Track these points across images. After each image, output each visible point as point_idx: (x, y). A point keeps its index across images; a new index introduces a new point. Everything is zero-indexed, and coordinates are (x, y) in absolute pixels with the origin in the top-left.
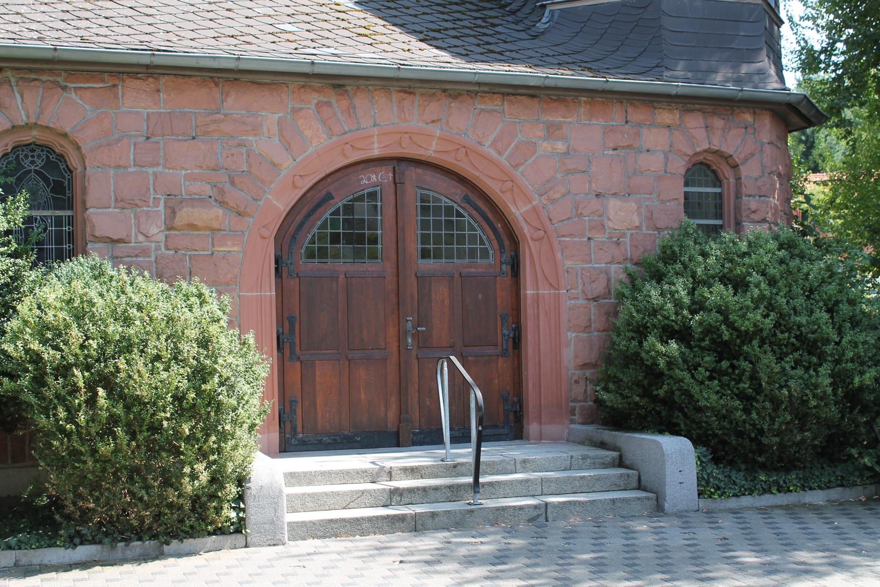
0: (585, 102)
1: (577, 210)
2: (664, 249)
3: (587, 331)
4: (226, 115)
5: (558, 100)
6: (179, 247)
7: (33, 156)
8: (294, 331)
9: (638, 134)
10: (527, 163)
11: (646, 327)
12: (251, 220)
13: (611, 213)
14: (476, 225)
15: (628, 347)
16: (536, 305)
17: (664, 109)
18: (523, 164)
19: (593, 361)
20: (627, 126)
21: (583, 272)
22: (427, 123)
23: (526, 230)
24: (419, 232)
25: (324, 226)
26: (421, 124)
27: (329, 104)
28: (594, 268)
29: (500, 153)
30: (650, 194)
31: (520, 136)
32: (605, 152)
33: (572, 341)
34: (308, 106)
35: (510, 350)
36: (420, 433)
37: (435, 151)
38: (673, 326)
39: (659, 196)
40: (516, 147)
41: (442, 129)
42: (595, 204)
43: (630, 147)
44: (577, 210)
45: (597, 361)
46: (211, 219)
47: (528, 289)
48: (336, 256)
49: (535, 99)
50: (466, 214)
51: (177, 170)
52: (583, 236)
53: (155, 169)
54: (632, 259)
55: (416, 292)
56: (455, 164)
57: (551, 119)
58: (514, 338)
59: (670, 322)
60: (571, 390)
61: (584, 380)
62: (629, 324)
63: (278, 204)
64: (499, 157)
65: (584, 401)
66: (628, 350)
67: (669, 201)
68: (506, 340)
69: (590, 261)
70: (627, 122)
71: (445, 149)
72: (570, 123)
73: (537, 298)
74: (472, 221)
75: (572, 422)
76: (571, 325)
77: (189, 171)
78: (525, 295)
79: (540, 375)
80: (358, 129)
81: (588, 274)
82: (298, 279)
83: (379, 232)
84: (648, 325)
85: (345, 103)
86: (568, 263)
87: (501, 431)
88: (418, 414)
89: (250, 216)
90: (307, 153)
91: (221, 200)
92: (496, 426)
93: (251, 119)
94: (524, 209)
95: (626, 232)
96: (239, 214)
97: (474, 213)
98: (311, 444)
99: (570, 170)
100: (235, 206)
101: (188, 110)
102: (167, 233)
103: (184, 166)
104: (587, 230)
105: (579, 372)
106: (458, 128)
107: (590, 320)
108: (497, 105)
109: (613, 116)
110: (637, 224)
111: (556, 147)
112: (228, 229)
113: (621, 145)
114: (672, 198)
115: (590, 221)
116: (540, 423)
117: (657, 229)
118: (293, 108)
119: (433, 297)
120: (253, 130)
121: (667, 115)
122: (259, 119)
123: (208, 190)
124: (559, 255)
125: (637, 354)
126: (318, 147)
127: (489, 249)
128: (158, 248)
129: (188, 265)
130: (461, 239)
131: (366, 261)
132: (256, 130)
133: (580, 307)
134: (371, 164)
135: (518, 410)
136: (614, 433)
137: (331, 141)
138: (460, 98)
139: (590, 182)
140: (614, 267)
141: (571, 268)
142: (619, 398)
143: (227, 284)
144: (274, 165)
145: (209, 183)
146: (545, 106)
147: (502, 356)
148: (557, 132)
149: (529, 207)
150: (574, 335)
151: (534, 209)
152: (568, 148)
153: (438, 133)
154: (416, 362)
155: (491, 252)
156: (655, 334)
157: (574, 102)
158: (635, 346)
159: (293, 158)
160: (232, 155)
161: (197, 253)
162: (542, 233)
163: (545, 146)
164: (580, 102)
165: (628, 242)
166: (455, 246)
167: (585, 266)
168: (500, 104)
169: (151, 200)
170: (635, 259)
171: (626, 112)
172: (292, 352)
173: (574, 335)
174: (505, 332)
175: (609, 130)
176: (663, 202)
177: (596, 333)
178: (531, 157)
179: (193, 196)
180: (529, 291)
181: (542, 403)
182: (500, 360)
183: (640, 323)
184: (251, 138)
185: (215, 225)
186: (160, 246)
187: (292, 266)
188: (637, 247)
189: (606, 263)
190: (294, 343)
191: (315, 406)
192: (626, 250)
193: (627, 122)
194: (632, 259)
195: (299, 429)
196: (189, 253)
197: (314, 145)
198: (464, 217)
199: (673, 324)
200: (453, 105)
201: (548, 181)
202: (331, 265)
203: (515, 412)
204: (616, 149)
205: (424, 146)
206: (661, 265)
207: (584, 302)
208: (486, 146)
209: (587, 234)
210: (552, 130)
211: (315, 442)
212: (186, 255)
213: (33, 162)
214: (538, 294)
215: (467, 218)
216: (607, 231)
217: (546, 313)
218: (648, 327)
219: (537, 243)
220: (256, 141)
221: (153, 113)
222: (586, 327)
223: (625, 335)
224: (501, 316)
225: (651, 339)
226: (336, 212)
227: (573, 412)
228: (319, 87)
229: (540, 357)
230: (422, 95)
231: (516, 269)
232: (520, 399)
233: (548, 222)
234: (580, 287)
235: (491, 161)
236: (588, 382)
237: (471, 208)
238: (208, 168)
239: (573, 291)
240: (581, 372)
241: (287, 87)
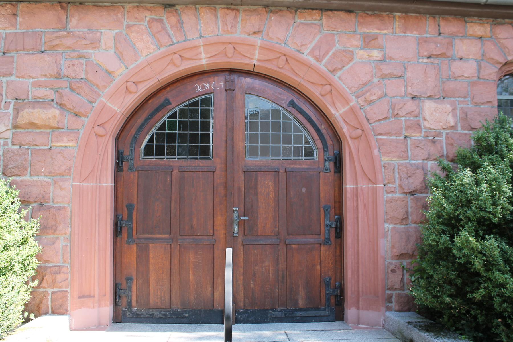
0: (399, 17)
1: (393, 110)
2: (479, 140)
3: (404, 223)
4: (68, 33)
5: (373, 15)
6: (23, 143)
8: (132, 218)
9: (450, 44)
10: (344, 68)
11: (459, 220)
12: (86, 120)
13: (427, 114)
14: (301, 127)
15: (437, 242)
16: (355, 198)
17: (475, 23)
18: (340, 69)
19: (410, 251)
20: (440, 37)
21: (400, 168)
22: (249, 35)
23: (345, 130)
24: (247, 132)
25: (162, 128)
26: (243, 36)
27: (160, 21)
28: (411, 164)
29: (318, 60)
30: (465, 97)
31: (337, 45)
32: (420, 60)
33: (390, 232)
34: (142, 23)
35: (333, 239)
36: (244, 313)
37: (259, 60)
38: (489, 219)
39: (473, 99)
40: (334, 54)
41: (263, 40)
42: (411, 106)
43: (442, 55)
44: (393, 110)
45: (413, 252)
46: (49, 118)
47: (347, 184)
48: (172, 153)
49: (352, 14)
50: (291, 117)
51: (25, 78)
52: (400, 134)
53: (8, 78)
54: (448, 157)
55: (243, 186)
56: (278, 72)
57: (367, 31)
58: (336, 228)
59: (488, 215)
60: (388, 279)
61: (401, 270)
62: (439, 216)
63: (113, 107)
64: (317, 64)
65: (401, 290)
66: (438, 245)
67: (483, 104)
68: (329, 230)
69: (407, 158)
70: (440, 34)
71: (267, 58)
72: (386, 34)
73: (356, 192)
74: (297, 124)
75: (389, 309)
76: (389, 217)
77: (36, 80)
78: (346, 188)
79: (358, 263)
80: (185, 41)
81: (405, 170)
82: (137, 172)
83: (281, 158)
84: (461, 217)
85: (174, 19)
86: (385, 159)
87: (322, 313)
88: (243, 295)
89: (85, 116)
90: (138, 62)
91: (60, 103)
92: (318, 309)
93: (91, 35)
94: (343, 110)
95: (442, 131)
96: (76, 115)
97: (300, 116)
98: (144, 317)
99: (386, 75)
100: (71, 107)
101: (39, 30)
102: (14, 131)
103: (31, 75)
104: (404, 129)
105: (396, 261)
106: (278, 38)
107: (407, 212)
108: (316, 20)
109: (427, 29)
110: (452, 124)
111: (371, 54)
112: (66, 128)
113: (435, 53)
114: (485, 101)
115: (405, 121)
116: (358, 308)
117: (473, 129)
118: (127, 25)
119: (259, 189)
120: (92, 43)
121: (478, 28)
122: (98, 34)
123: (51, 94)
124: (376, 152)
125: (448, 250)
126: (148, 57)
127: (314, 148)
129: (30, 158)
130: (287, 140)
131: (199, 157)
132: (95, 44)
133: (397, 201)
134: (206, 75)
135: (339, 294)
136: (422, 334)
137: (160, 51)
138: (280, 13)
139: (406, 86)
140: (430, 164)
141: (388, 164)
142: (429, 297)
143: (61, 175)
144: (109, 73)
145: (52, 89)
146: (361, 20)
147: (324, 244)
148: (373, 42)
149: (348, 107)
150: (391, 226)
151: (352, 109)
152: (384, 56)
153: (259, 42)
154: (242, 248)
155: (315, 151)
156: (469, 227)
157: (389, 17)
158: (446, 241)
159: (125, 66)
160: (73, 65)
161: (38, 148)
162: (360, 131)
163: (361, 54)
164: (394, 17)
165: (444, 141)
166: (281, 145)
167: (401, 162)
168: (319, 18)
170: (451, 156)
171: (439, 25)
172: (130, 235)
173: (391, 226)
174: (328, 222)
175: (422, 42)
176: (476, 104)
177: (413, 225)
178: (348, 63)
179: (38, 100)
180: (349, 186)
181: (360, 289)
182: (323, 248)
183: (452, 216)
184: (90, 51)
185: (54, 124)
186: (7, 142)
187: (132, 162)
188: (452, 145)
189: (423, 160)
190: (132, 229)
191: (148, 284)
192: (442, 148)
193: (440, 34)
194: (448, 157)
195: (134, 303)
196: (32, 148)
197: (144, 55)
198: (290, 119)
199: (491, 216)
200: (273, 18)
201: (365, 84)
202: (165, 161)
203: (336, 296)
204: (430, 57)
205: (248, 55)
206: (476, 157)
207: (401, 196)
208: (305, 53)
209: (404, 132)
211: (147, 316)
212: (28, 149)
214: (357, 188)
215: (293, 121)
216: (424, 130)
217: (365, 205)
218: (461, 220)
219: (356, 141)
220: (94, 53)
221: (10, 33)
222: (403, 219)
223: (434, 228)
224: (323, 208)
225: (465, 233)
226: (174, 116)
227: (389, 299)
228: (151, 7)
229: (358, 247)
230: (245, 11)
231: (338, 166)
232: (341, 284)
233: (365, 122)
234: (397, 182)
235: (309, 66)
236: (405, 271)
237: (296, 112)
238: (51, 76)
239: (390, 185)
240: (398, 261)
241: (124, 8)
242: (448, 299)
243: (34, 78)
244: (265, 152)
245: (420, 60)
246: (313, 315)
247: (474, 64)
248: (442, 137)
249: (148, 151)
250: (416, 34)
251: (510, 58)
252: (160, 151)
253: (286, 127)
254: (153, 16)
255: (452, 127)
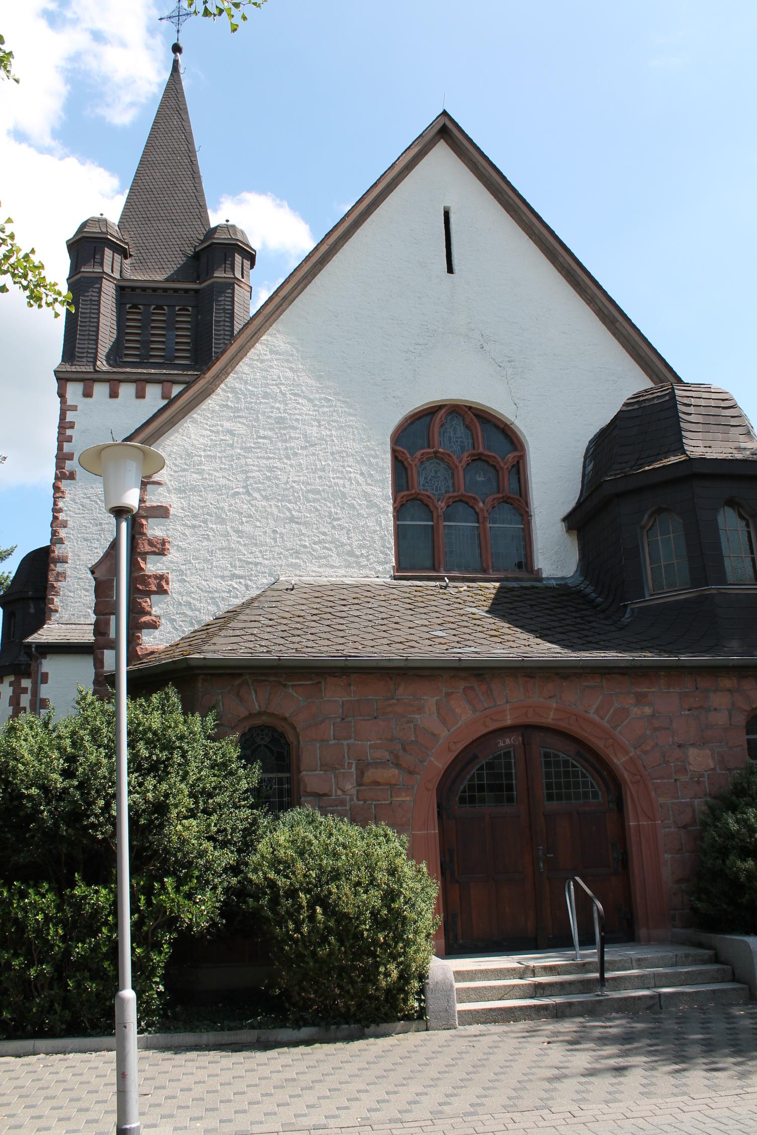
2: (735, 785)
7: (262, 735)
12: (419, 777)
13: (691, 759)
27: (472, 688)
29: (602, 718)
37: (552, 719)
43: (701, 707)
53: (348, 742)
54: (710, 795)
69: (678, 798)
70: (697, 689)
72: (654, 692)
74: (584, 771)
75: (674, 926)
78: (629, 825)
86: (661, 800)
90: (458, 725)
96: (410, 773)
110: (712, 766)
117: (729, 770)
124: (653, 794)
127: (599, 791)
128: (351, 800)
132: (420, 710)
139: (673, 736)
144: (434, 735)
150: (670, 856)
155: (600, 794)
163: (636, 711)
165: (707, 781)
169: (346, 764)
173: (670, 856)
177: (687, 854)
184: (417, 716)
193: (697, 689)
194: (710, 795)
206: (734, 798)
210: (640, 699)
212: (371, 804)
213: (262, 739)
214: (639, 825)
225: (732, 858)
226: (481, 768)
242: (725, 906)
243: (371, 741)
244: (559, 798)
245: (683, 713)
246: (478, 1033)
247: (727, 712)
248: (704, 777)
249: (462, 800)
250: (678, 690)
251: (754, 706)
252: (472, 800)
253: (575, 774)
254: (467, 685)
255: (712, 769)
